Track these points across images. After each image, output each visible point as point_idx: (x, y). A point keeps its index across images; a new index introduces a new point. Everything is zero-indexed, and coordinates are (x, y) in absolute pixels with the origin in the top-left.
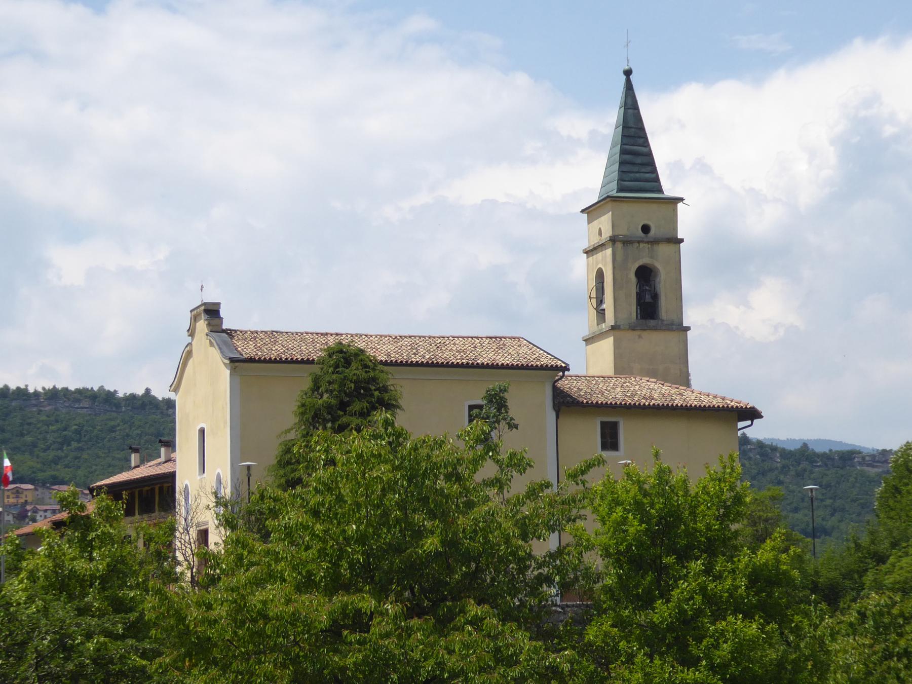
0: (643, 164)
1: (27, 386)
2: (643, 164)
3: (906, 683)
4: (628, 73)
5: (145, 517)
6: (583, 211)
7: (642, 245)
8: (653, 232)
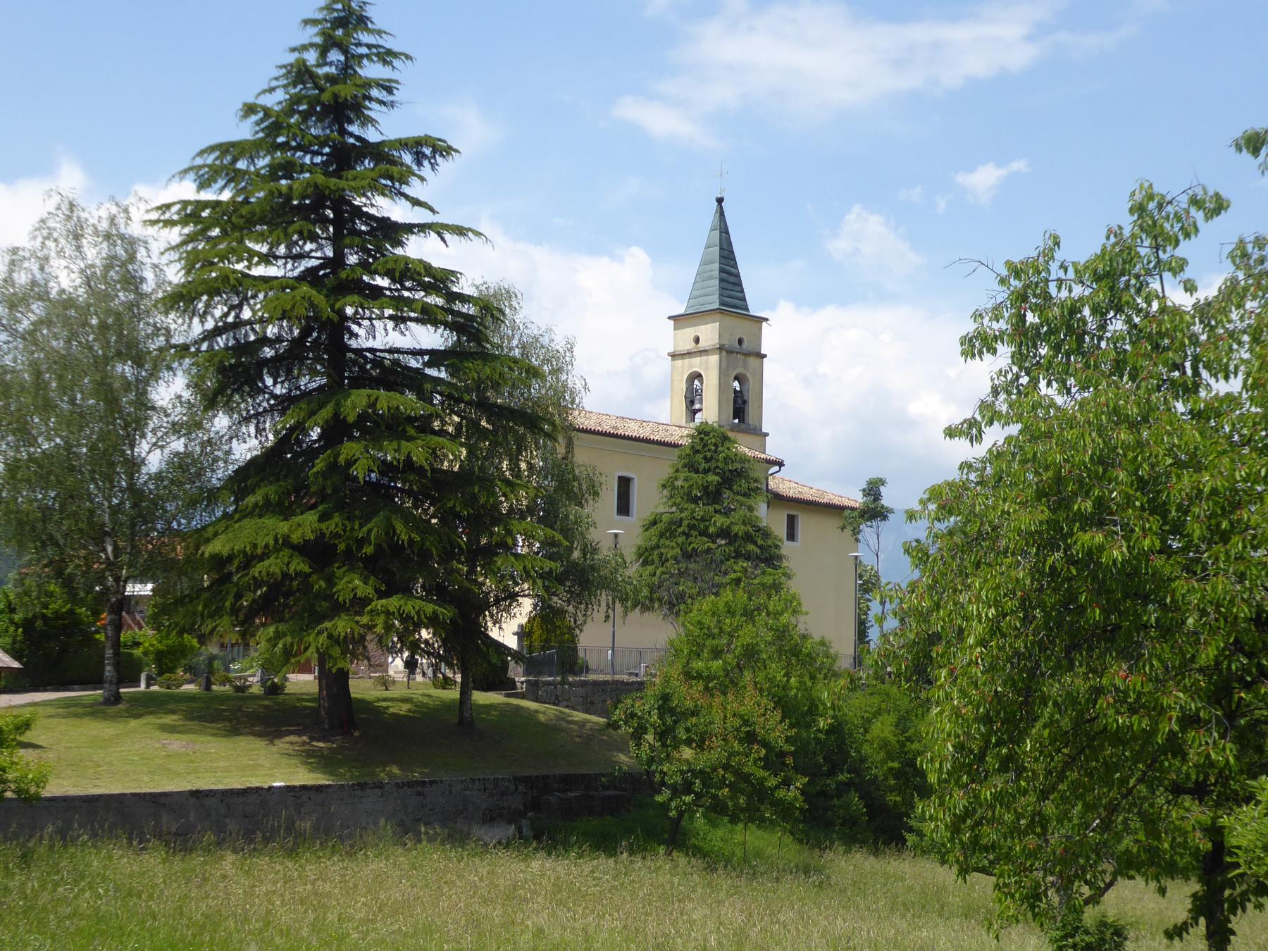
0: (734, 284)
1: (514, 634)
2: (734, 284)
3: (1129, 946)
4: (720, 201)
5: (638, 858)
6: (670, 318)
7: (739, 356)
8: (745, 345)
